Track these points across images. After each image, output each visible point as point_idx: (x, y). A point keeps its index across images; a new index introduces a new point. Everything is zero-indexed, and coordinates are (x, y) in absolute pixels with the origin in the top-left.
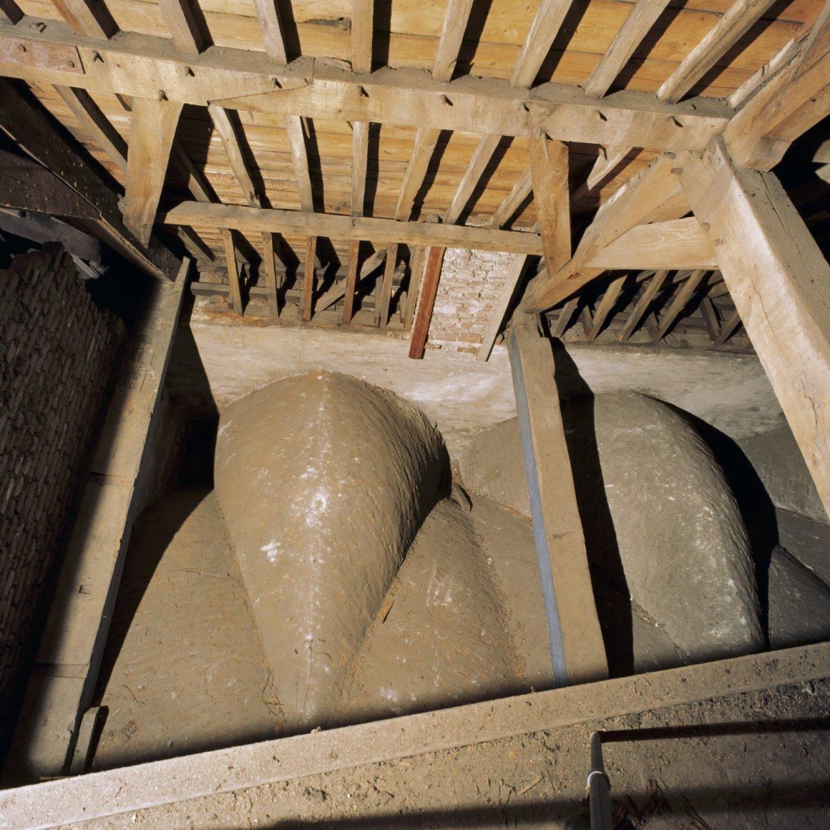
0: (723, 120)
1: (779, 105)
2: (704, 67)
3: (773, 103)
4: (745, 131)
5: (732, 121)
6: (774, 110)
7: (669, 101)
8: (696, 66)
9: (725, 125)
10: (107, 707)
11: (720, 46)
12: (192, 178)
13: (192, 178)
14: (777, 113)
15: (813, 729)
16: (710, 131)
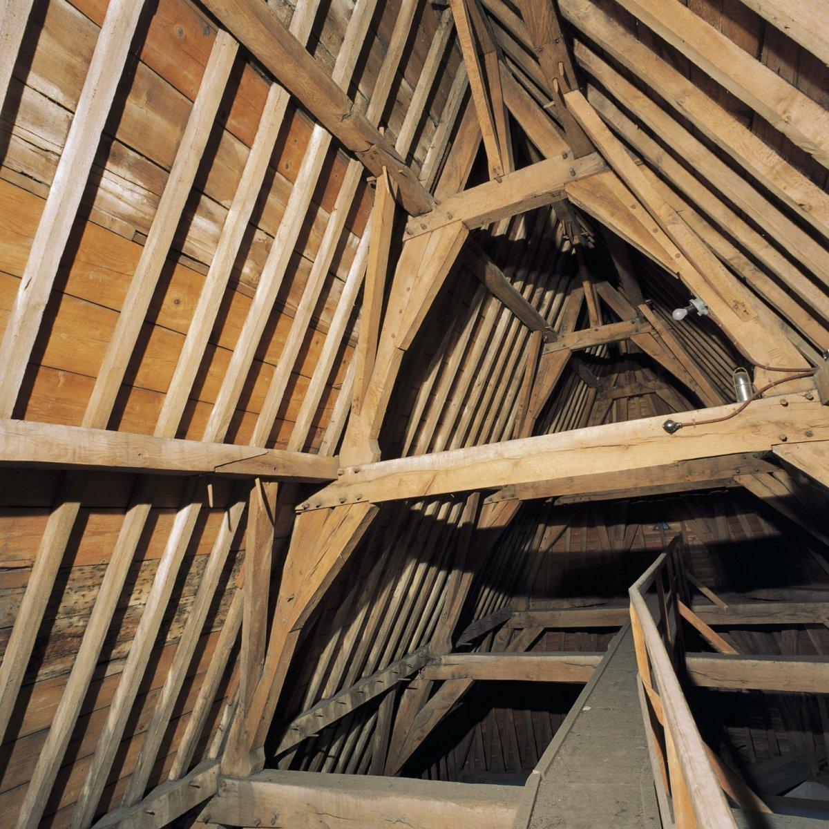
0: (217, 766)
1: (246, 732)
2: (195, 742)
3: (242, 734)
4: (236, 759)
5: (222, 763)
6: (245, 736)
7: (181, 777)
8: (191, 745)
9: (220, 768)
10: (524, 785)
11: (205, 711)
12: (307, 757)
13: (307, 757)
14: (249, 736)
15: (539, 640)
16: (214, 777)
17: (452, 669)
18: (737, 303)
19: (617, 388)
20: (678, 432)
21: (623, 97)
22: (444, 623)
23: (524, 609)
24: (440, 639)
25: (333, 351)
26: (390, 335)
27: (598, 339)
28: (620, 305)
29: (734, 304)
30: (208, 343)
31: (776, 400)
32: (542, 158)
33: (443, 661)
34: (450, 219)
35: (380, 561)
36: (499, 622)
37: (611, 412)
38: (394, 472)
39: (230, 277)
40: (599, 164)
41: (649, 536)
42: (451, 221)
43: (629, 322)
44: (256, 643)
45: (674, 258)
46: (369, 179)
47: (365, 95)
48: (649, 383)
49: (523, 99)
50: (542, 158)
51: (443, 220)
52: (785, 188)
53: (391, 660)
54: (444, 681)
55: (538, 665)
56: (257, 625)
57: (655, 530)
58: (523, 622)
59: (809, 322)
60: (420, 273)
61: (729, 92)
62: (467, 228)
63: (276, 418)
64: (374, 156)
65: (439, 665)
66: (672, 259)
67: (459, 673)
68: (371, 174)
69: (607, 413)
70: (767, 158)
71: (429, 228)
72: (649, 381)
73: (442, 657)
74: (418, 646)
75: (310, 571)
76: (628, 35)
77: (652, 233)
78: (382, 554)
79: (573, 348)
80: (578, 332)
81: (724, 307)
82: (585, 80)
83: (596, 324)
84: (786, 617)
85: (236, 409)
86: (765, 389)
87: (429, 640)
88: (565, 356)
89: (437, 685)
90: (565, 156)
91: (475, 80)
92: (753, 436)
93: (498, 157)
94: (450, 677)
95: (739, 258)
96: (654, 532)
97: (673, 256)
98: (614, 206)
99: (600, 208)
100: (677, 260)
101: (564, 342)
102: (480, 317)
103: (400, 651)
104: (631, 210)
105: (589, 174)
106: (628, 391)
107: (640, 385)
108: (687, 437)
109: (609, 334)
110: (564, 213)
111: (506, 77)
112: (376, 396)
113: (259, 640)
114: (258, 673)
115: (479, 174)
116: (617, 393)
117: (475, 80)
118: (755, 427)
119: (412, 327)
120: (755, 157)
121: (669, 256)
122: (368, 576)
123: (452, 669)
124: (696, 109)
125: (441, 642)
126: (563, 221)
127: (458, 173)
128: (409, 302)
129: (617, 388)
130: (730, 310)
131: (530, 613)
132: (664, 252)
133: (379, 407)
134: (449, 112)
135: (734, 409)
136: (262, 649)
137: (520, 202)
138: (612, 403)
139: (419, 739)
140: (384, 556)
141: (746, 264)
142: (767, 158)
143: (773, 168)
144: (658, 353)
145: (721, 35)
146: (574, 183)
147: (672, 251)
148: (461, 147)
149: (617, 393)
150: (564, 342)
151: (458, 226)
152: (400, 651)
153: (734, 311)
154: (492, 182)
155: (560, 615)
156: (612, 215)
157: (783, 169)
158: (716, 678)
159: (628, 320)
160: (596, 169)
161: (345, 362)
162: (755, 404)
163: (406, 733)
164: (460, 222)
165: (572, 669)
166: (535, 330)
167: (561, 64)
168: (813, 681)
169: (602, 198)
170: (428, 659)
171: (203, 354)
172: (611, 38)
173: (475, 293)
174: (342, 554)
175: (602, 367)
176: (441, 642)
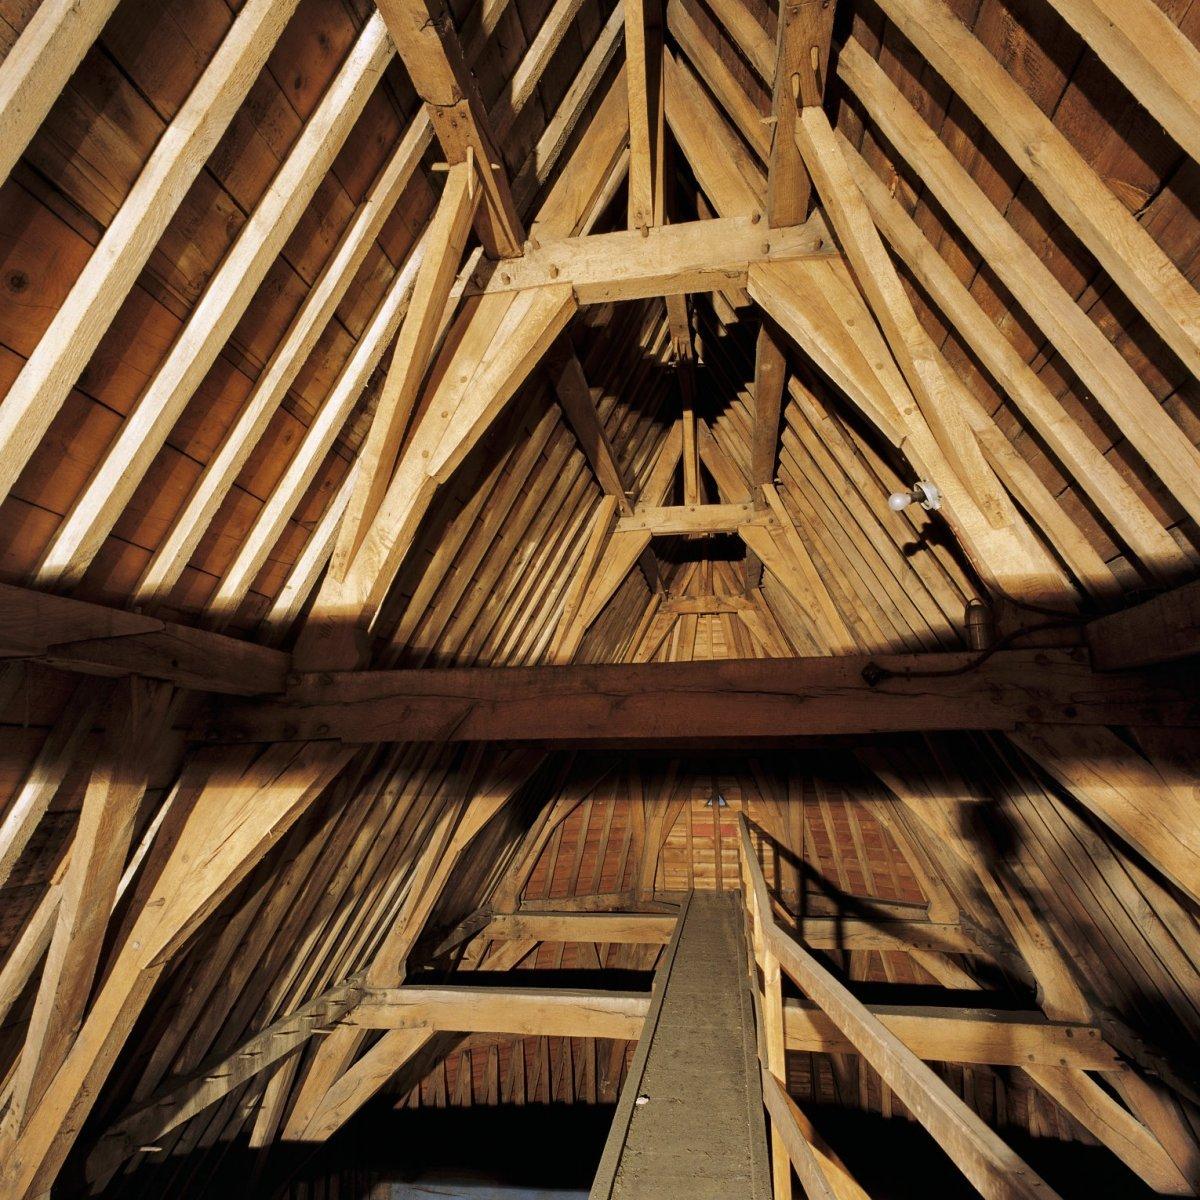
6: (13, 1174)
14: (21, 1174)
17: (404, 1011)
18: (990, 498)
19: (687, 599)
20: (884, 686)
21: (900, 133)
22: (398, 936)
23: (511, 911)
24: (388, 962)
25: (318, 452)
26: (420, 452)
27: (693, 524)
28: (728, 478)
29: (985, 500)
30: (75, 388)
31: (1027, 655)
32: (714, 215)
33: (389, 998)
34: (553, 278)
35: (319, 837)
36: (473, 931)
37: (672, 637)
38: (397, 692)
39: (147, 265)
40: (806, 245)
41: (698, 814)
42: (554, 281)
43: (740, 506)
44: (71, 992)
45: (903, 414)
46: (437, 167)
47: (456, 14)
48: (731, 599)
49: (696, 116)
50: (714, 215)
51: (540, 276)
52: (1183, 322)
53: (305, 1000)
54: (385, 1032)
55: (542, 1011)
56: (80, 958)
57: (707, 805)
58: (507, 931)
59: (1080, 545)
60: (487, 357)
61: (1167, 132)
62: (577, 300)
63: (188, 566)
64: (460, 121)
65: (381, 1004)
66: (899, 414)
67: (414, 1020)
68: (443, 159)
69: (666, 636)
70: (1161, 268)
71: (514, 284)
72: (731, 595)
73: (388, 992)
74: (350, 972)
75: (206, 855)
76: (956, 21)
77: (874, 369)
78: (325, 823)
79: (654, 531)
80: (666, 508)
81: (967, 501)
82: (837, 97)
83: (693, 502)
84: (865, 941)
85: (111, 535)
86: (1016, 635)
87: (370, 961)
88: (643, 539)
89: (373, 1037)
90: (757, 219)
91: (637, 55)
92: (992, 704)
93: (644, 196)
94: (398, 1025)
95: (994, 432)
96: (705, 809)
97: (901, 410)
98: (823, 318)
99: (799, 314)
100: (907, 419)
101: (644, 520)
102: (511, 463)
103: (322, 983)
104: (847, 326)
105: (789, 256)
106: (700, 605)
107: (719, 599)
108: (896, 694)
109: (710, 520)
110: (681, 326)
111: (673, 75)
112: (379, 553)
113: (78, 986)
114: (63, 1050)
115: (613, 218)
116: (686, 605)
117: (637, 55)
118: (996, 692)
119: (461, 446)
120: (1142, 263)
121: (896, 409)
122: (294, 860)
123: (404, 1011)
124: (1057, 166)
125: (389, 967)
126: (676, 339)
127: (575, 206)
128: (462, 400)
129: (687, 599)
130: (975, 508)
131: (519, 917)
132: (887, 400)
133: (383, 573)
134: (570, 104)
135: (969, 660)
136: (80, 1003)
137: (675, 276)
138: (678, 618)
139: (329, 1128)
140: (327, 828)
141: (1002, 443)
142: (1161, 268)
143: (1167, 286)
144: (773, 557)
145: (1177, 32)
146: (764, 266)
147: (901, 400)
148: (584, 165)
149: (686, 605)
150: (644, 520)
151: (565, 294)
152: (322, 983)
153: (982, 511)
154: (631, 234)
155: (564, 922)
156: (817, 328)
157: (1183, 291)
158: (797, 1037)
159: (739, 503)
160: (799, 252)
161: (328, 484)
162: (999, 657)
163: (307, 1118)
164: (569, 286)
165: (594, 1016)
166: (610, 494)
167: (814, 51)
168: (920, 1043)
169: (805, 298)
170: (362, 993)
171: (60, 405)
172: (927, 17)
173: (543, 416)
174: (272, 831)
175: (670, 566)
176: (389, 967)
